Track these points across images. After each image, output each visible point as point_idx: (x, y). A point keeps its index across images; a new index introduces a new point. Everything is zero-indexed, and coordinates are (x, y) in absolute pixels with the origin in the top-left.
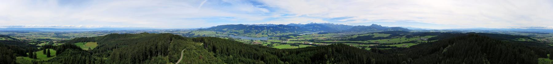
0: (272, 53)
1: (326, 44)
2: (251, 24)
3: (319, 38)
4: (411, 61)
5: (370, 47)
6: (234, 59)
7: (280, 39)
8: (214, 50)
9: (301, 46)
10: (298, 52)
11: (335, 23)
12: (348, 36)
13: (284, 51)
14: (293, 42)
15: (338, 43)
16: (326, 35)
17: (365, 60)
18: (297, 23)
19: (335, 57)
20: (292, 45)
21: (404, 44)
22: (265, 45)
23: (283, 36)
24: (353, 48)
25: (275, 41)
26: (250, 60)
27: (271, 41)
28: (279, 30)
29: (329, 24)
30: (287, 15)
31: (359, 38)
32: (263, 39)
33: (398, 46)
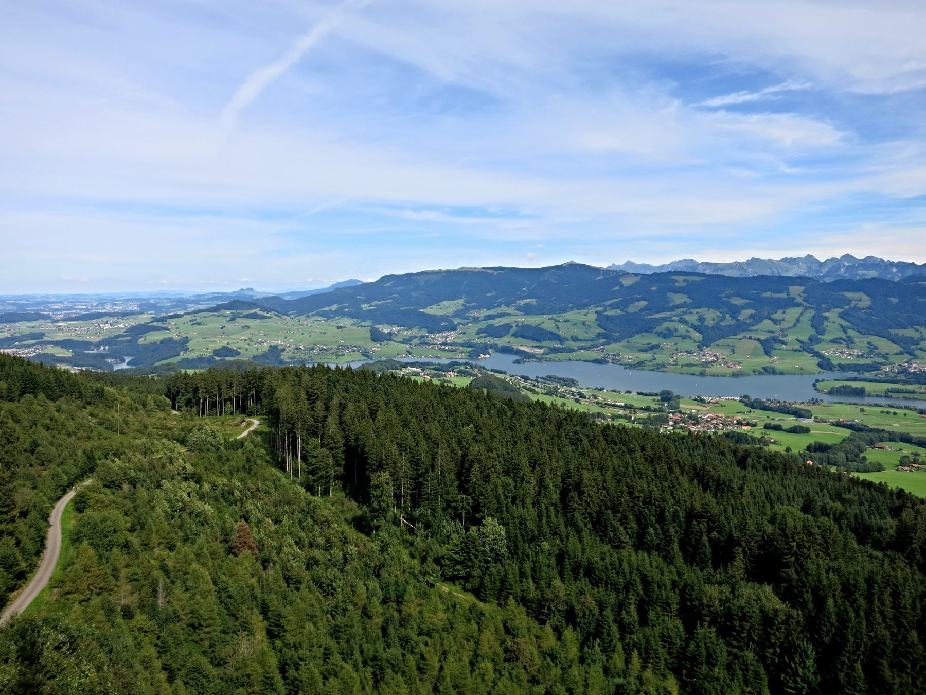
0: (863, 532)
2: (659, 259)
6: (513, 551)
8: (356, 472)
22: (782, 444)
25: (896, 426)
26: (650, 563)
27: (847, 411)
32: (761, 390)
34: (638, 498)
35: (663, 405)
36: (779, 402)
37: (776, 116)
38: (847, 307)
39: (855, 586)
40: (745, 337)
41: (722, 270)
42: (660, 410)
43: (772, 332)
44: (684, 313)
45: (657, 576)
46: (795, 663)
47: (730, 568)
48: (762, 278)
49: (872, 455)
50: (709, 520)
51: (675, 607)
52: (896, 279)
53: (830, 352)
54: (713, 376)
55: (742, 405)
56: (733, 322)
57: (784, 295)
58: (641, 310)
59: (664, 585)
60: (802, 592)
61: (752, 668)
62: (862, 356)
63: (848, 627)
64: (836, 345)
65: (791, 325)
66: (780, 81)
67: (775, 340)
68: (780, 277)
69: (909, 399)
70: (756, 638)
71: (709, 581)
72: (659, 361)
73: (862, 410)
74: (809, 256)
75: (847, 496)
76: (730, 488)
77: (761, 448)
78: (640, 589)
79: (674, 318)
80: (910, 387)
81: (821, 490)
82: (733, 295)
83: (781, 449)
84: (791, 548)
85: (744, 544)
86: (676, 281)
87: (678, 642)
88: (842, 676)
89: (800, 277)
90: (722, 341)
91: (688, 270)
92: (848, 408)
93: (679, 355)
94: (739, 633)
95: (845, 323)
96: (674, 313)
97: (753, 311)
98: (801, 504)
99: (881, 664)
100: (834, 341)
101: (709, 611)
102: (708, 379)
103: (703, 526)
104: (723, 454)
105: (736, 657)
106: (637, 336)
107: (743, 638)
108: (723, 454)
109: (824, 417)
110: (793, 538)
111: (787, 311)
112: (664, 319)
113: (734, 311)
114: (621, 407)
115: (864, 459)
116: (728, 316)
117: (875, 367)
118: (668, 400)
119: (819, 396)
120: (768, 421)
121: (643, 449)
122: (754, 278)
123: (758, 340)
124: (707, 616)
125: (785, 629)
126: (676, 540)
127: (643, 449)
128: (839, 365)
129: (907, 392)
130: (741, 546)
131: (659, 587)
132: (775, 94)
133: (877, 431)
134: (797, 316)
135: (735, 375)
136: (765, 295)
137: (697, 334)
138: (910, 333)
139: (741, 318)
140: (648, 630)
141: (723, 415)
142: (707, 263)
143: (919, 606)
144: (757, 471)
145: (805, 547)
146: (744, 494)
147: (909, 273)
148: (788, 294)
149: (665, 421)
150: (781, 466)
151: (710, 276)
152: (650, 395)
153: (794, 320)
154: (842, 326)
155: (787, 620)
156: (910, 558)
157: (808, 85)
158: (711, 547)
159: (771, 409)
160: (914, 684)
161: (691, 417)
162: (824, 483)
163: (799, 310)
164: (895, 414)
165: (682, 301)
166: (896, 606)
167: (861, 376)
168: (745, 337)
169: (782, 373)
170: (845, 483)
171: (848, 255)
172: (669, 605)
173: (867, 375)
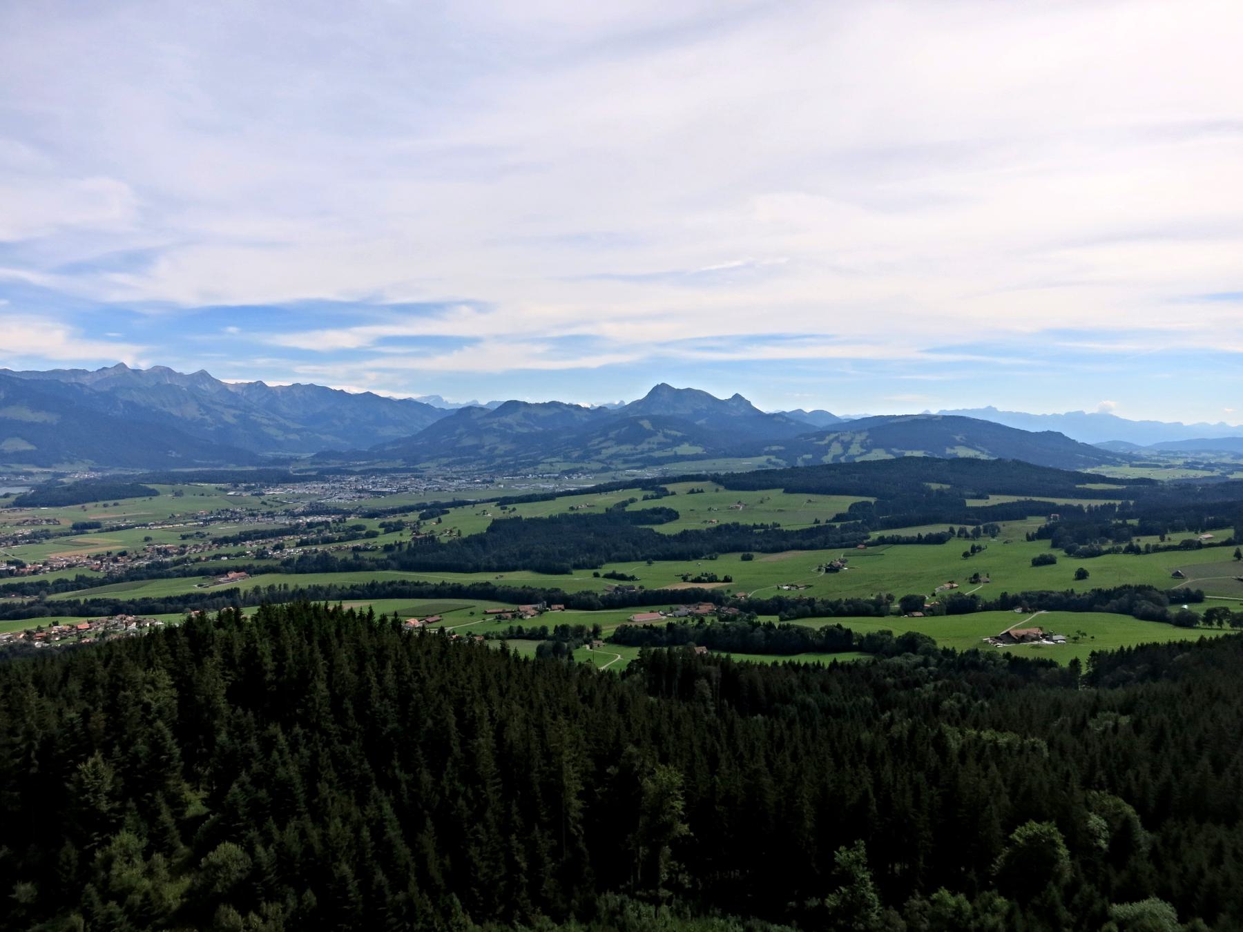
3: (31, 555)
4: (1122, 837)
5: (623, 637)
12: (390, 519)
15: (265, 600)
16: (131, 508)
17: (572, 782)
19: (230, 766)
21: (1017, 622)
24: (444, 647)
31: (510, 542)
33: (952, 634)
41: (1113, 463)
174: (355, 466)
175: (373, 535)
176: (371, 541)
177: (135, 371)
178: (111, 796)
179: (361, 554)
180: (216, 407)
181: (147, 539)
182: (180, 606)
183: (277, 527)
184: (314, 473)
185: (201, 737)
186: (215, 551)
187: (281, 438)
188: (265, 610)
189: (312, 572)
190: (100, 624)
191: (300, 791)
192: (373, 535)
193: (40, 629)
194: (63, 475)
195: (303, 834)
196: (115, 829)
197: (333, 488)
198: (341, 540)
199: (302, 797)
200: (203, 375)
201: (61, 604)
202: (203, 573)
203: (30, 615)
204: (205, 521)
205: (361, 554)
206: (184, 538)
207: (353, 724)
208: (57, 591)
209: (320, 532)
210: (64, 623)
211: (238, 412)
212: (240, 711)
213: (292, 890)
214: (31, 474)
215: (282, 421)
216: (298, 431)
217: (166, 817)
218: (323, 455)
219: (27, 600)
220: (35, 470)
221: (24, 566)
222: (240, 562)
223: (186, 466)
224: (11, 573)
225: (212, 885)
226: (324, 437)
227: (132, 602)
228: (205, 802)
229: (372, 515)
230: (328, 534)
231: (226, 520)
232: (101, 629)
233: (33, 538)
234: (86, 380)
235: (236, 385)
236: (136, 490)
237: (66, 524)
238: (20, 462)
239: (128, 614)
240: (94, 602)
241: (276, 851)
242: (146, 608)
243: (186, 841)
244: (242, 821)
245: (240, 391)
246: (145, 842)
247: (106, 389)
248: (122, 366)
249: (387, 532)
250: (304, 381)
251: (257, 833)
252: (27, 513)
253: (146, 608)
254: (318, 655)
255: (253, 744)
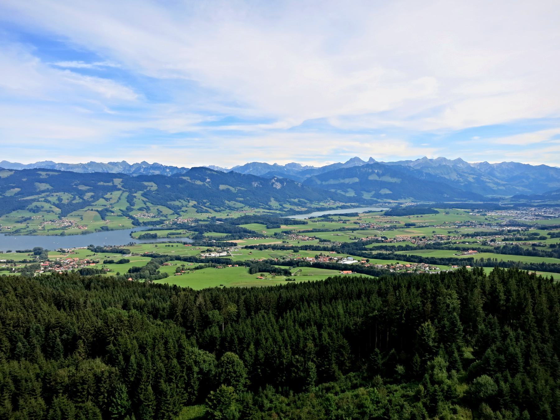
0: (155, 313)
1: (426, 268)
2: (27, 159)
7: (197, 240)
9: (300, 276)
10: (285, 302)
11: (473, 159)
13: (215, 297)
14: (262, 257)
16: (428, 218)
18: (282, 163)
20: (255, 268)
22: (116, 271)
23: (211, 228)
25: (173, 252)
27: (149, 248)
28: (193, 193)
29: (441, 163)
30: (230, 120)
34: (9, 325)
35: (36, 257)
36: (111, 247)
37: (101, 80)
38: (145, 190)
39: (146, 344)
40: (89, 210)
41: (72, 168)
42: (34, 261)
43: (105, 206)
44: (48, 196)
45: (24, 374)
46: (116, 398)
47: (74, 355)
48: (97, 174)
49: (162, 270)
50: (61, 327)
51: (38, 391)
52: (169, 175)
53: (138, 215)
54: (70, 235)
55: (89, 251)
56: (81, 201)
57: (110, 184)
58: (16, 194)
59: (30, 379)
60: (117, 357)
61: (91, 411)
62: (154, 217)
63: (142, 368)
64: (141, 212)
65: (116, 201)
66: (99, 59)
67: (107, 210)
68: (108, 174)
69: (178, 237)
70: (92, 392)
71: (61, 367)
72: (31, 228)
73: (156, 246)
74: (124, 162)
75: (148, 294)
76: (78, 304)
77: (99, 276)
78: (13, 387)
79: (40, 199)
80: (178, 231)
81: (134, 294)
82: (80, 184)
83: (114, 274)
84: (111, 332)
85: (83, 337)
86: (41, 175)
87: (42, 413)
88: (142, 396)
89: (119, 174)
90: (74, 213)
91: (49, 168)
92: (149, 246)
93: (46, 223)
94: (81, 392)
95: (145, 199)
96: (40, 196)
97: (92, 194)
98: (122, 304)
99: (160, 382)
100: (140, 209)
101: (62, 386)
102: (66, 237)
103: (57, 333)
104: (76, 283)
105: (81, 408)
106: (14, 212)
107: (84, 395)
108: (76, 283)
109: (137, 252)
110: (112, 326)
111: (113, 193)
112: (34, 200)
113: (81, 194)
114: (4, 262)
115: (159, 272)
116: (77, 197)
117: (161, 222)
118: (40, 254)
119: (133, 241)
120: (106, 259)
121: (15, 289)
122: (92, 173)
123: (97, 211)
124: (61, 389)
125: (109, 381)
126: (38, 346)
127: (15, 289)
128: (143, 222)
129: (178, 234)
130: (81, 339)
131: (26, 381)
132: (101, 67)
133: (164, 256)
134: (119, 196)
135: (84, 233)
136: (99, 184)
137: (58, 209)
138: (177, 203)
139: (85, 198)
140: (18, 413)
141: (78, 259)
142: (62, 164)
143: (177, 346)
144: (97, 290)
145: (119, 329)
146: (87, 306)
147: (175, 172)
148: (113, 183)
149: (38, 267)
150: (111, 284)
151: (64, 172)
152: (26, 252)
153: (117, 199)
154: (143, 201)
155: (110, 375)
156: (176, 321)
157: (119, 66)
158: (63, 344)
159: (107, 252)
160: (177, 387)
161: (56, 263)
162: (136, 290)
163: (119, 193)
164: (172, 246)
165: (46, 188)
166: (166, 349)
167: (155, 228)
168: (89, 210)
169: (112, 230)
170: (147, 287)
171: (144, 162)
172: (34, 391)
173: (158, 227)
174: (535, 202)
175: (544, 238)
176: (542, 241)
177: (430, 160)
178: (434, 339)
179: (536, 248)
180: (465, 174)
181: (434, 232)
182: (447, 262)
183: (492, 231)
184: (512, 206)
185: (471, 324)
186: (463, 240)
187: (495, 189)
188: (496, 271)
189: (509, 254)
190: (415, 265)
191: (521, 360)
192: (544, 238)
193: (392, 265)
194: (402, 204)
195: (523, 383)
196: (436, 354)
197: (522, 213)
198: (525, 240)
199: (522, 364)
200: (460, 160)
201: (400, 256)
202: (457, 249)
203: (389, 259)
204: (459, 226)
205: (536, 248)
206: (449, 233)
207: (547, 334)
208: (399, 250)
209: (514, 235)
210: (401, 263)
211: (475, 176)
212: (491, 316)
213: (517, 407)
214: (390, 203)
215: (496, 180)
216: (504, 185)
217: (456, 354)
218: (517, 197)
219: (388, 252)
220: (392, 201)
221: (387, 239)
222: (474, 246)
223: (451, 201)
224: (382, 241)
225: (479, 392)
226: (517, 188)
227: (427, 258)
228: (473, 353)
229: (543, 228)
230: (518, 236)
231: (468, 226)
232: (415, 268)
233: (391, 228)
234: (411, 165)
235: (474, 164)
236: (430, 211)
237: (403, 224)
238: (386, 198)
239: (425, 263)
240: (412, 256)
241: (510, 387)
242: (433, 261)
243: (464, 369)
244: (491, 367)
245: (476, 167)
246: (447, 364)
247: (419, 168)
248: (425, 158)
249: (552, 237)
250: (508, 161)
251: (500, 375)
252: (389, 218)
253: (433, 261)
254: (528, 296)
255: (497, 332)
